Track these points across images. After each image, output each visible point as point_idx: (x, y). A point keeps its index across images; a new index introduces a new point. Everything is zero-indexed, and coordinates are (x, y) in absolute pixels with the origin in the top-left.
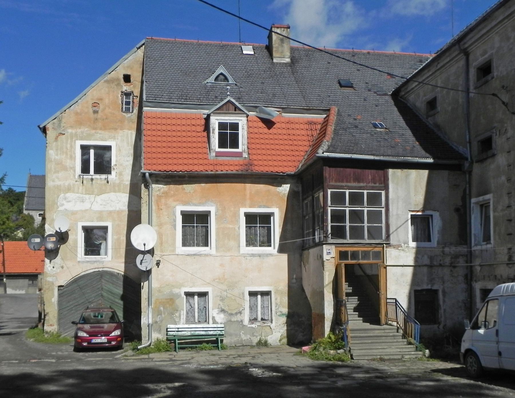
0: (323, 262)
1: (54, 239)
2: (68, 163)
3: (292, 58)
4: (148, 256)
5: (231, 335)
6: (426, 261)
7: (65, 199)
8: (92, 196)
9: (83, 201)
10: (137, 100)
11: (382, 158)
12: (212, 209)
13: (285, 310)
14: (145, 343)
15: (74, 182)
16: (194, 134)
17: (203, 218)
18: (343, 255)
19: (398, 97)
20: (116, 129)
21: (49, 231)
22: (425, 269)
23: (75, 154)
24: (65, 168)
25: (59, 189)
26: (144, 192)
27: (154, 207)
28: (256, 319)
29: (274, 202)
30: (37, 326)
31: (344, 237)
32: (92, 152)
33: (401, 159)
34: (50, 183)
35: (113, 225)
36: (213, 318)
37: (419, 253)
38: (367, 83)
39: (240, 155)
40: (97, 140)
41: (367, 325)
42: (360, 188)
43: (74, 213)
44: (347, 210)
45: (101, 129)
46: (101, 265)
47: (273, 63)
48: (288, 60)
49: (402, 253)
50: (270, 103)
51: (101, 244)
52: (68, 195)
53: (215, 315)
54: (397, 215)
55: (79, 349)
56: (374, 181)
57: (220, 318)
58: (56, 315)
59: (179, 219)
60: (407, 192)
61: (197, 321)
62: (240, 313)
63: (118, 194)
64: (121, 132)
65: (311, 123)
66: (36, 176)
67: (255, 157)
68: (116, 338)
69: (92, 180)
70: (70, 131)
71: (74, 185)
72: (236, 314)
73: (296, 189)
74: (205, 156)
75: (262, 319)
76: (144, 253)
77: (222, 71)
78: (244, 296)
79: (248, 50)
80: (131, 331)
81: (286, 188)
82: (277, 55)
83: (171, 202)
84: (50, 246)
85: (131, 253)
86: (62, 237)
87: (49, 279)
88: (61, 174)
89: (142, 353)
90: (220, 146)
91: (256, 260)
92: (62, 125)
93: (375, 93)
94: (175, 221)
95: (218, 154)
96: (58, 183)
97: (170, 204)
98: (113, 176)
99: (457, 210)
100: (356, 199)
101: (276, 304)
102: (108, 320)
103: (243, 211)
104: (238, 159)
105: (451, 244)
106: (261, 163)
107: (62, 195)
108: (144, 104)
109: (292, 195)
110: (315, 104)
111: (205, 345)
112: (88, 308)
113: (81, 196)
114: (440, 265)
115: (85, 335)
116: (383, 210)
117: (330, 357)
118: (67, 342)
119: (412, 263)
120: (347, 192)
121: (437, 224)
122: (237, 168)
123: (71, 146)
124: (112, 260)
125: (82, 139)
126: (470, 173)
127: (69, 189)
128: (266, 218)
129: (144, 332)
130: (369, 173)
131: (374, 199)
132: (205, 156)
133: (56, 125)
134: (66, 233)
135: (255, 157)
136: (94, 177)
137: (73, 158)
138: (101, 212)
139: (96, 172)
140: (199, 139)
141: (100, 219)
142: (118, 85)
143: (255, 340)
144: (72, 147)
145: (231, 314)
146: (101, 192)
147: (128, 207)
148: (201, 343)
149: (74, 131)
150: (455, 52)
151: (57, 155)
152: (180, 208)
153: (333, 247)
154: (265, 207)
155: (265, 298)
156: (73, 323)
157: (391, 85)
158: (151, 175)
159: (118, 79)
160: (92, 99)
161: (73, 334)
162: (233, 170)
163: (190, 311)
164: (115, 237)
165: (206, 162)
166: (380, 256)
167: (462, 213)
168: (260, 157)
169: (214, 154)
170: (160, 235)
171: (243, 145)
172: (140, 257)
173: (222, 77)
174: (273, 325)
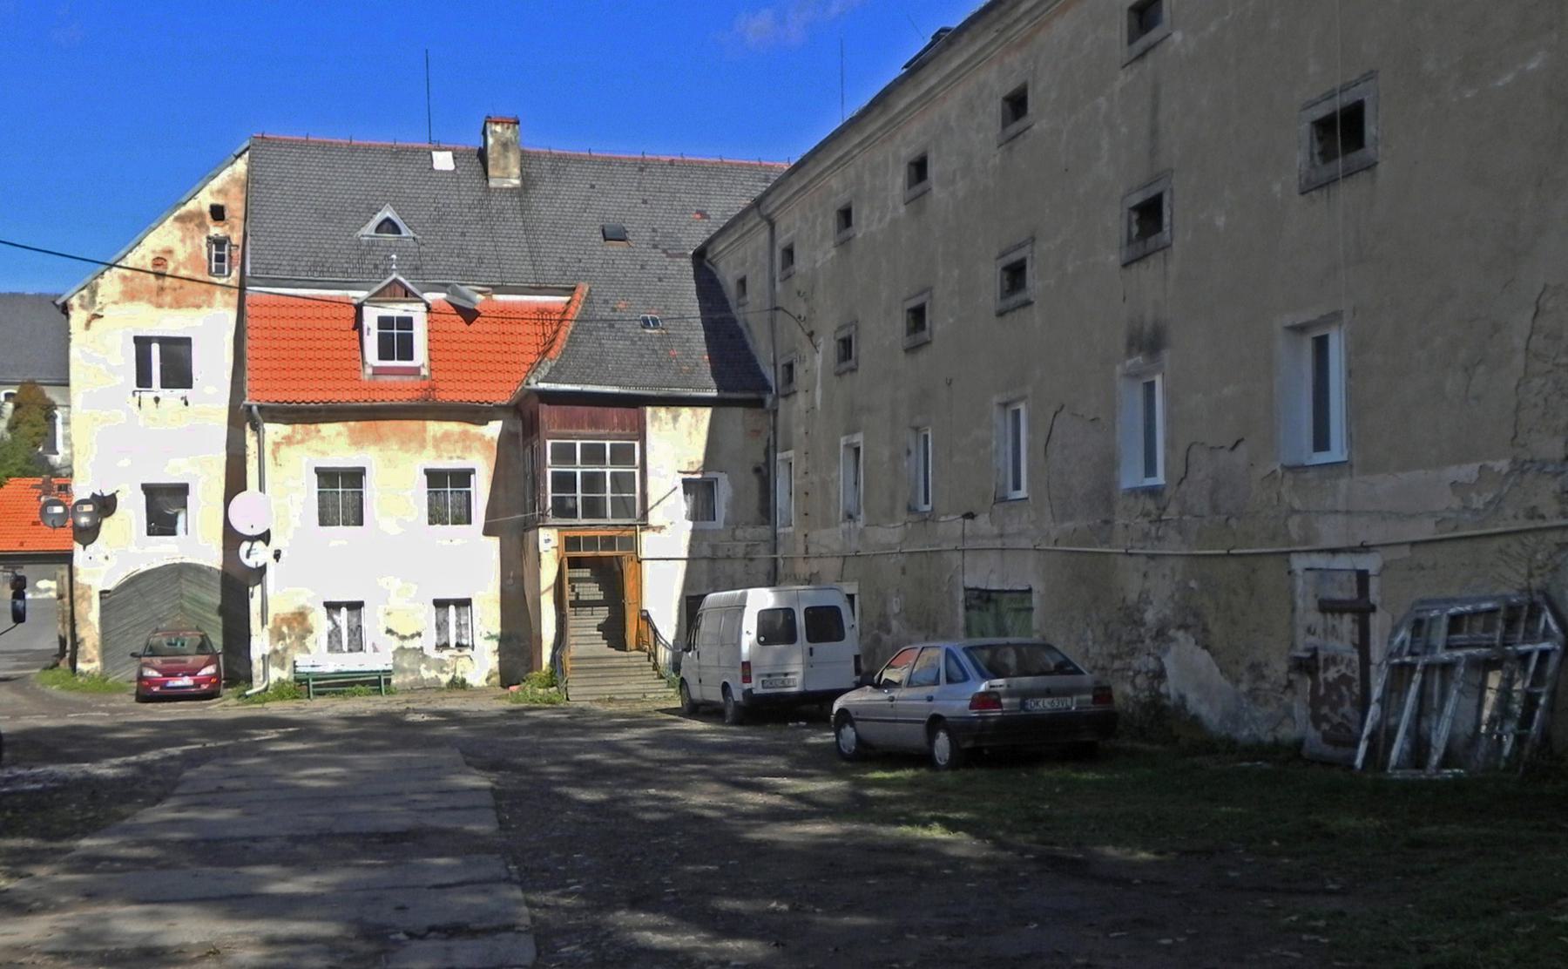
0: (539, 554)
1: (89, 508)
3: (524, 177)
4: (259, 545)
5: (404, 671)
6: (706, 551)
10: (237, 254)
11: (632, 391)
13: (497, 630)
14: (258, 686)
16: (337, 334)
17: (355, 477)
18: (571, 543)
20: (198, 307)
22: (704, 564)
26: (251, 440)
28: (446, 646)
29: (475, 450)
30: (57, 665)
32: (155, 349)
33: (664, 392)
37: (696, 536)
38: (654, 230)
39: (415, 371)
41: (613, 652)
44: (579, 472)
45: (171, 307)
47: (487, 189)
48: (516, 182)
50: (469, 275)
51: (176, 515)
55: (144, 697)
56: (622, 426)
60: (676, 443)
61: (345, 648)
65: (542, 313)
67: (441, 375)
68: (209, 678)
72: (413, 636)
73: (512, 429)
75: (459, 645)
76: (253, 539)
79: (443, 161)
80: (236, 671)
81: (494, 429)
84: (84, 520)
85: (232, 538)
86: (105, 505)
89: (253, 702)
90: (381, 358)
92: (98, 299)
93: (665, 251)
95: (378, 371)
97: (293, 461)
99: (757, 470)
100: (594, 454)
102: (195, 650)
105: (747, 524)
106: (451, 385)
108: (247, 281)
109: (505, 439)
111: (359, 687)
112: (157, 630)
114: (728, 557)
115: (155, 674)
116: (637, 472)
117: (536, 698)
118: (120, 689)
119: (685, 554)
120: (578, 443)
121: (724, 492)
122: (409, 395)
124: (198, 542)
126: (775, 412)
128: (463, 477)
129: (257, 667)
130: (614, 414)
131: (622, 455)
134: (113, 497)
135: (441, 375)
140: (345, 344)
142: (202, 225)
143: (445, 679)
145: (404, 638)
147: (228, 447)
148: (352, 684)
150: (754, 219)
153: (555, 531)
155: (462, 610)
156: (133, 655)
157: (696, 236)
158: (260, 408)
159: (200, 214)
161: (133, 674)
162: (401, 398)
163: (334, 635)
166: (631, 544)
167: (764, 475)
169: (369, 371)
172: (245, 546)
173: (389, 226)
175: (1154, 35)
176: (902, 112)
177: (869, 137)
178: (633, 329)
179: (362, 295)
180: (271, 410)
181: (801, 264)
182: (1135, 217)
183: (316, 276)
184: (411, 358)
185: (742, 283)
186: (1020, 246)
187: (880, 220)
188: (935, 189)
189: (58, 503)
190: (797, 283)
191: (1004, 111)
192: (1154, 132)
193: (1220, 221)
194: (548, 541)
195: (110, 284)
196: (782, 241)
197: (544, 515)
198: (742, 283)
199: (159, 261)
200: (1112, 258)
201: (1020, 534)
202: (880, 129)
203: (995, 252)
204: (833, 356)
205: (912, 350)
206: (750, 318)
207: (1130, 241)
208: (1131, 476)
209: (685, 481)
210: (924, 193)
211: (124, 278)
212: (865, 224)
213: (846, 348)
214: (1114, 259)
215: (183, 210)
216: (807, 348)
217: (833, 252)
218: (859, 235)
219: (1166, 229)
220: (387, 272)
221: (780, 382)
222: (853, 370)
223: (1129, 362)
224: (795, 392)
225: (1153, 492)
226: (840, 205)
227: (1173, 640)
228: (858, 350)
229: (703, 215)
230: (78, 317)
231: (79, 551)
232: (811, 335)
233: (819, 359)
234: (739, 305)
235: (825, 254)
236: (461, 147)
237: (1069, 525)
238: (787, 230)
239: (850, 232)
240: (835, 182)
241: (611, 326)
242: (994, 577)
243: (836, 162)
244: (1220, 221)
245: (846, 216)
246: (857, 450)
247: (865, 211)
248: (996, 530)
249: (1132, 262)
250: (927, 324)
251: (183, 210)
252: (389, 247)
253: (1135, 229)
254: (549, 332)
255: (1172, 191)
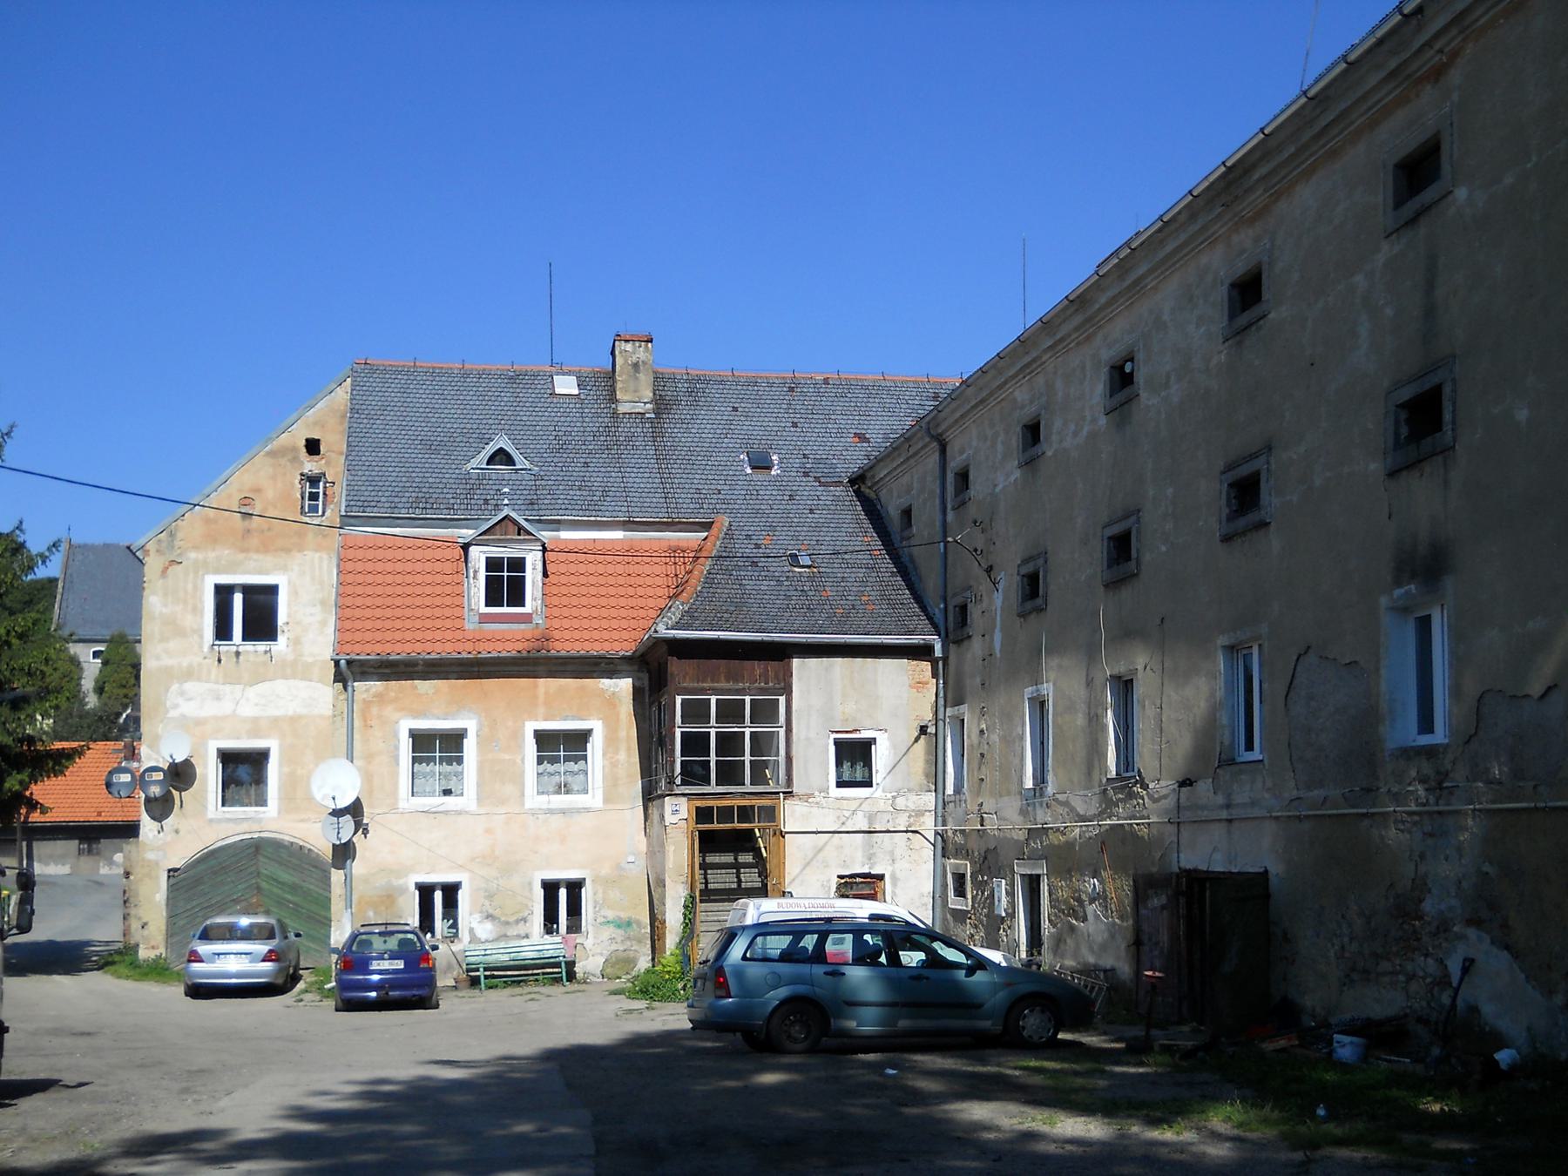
2: (188, 621)
7: (182, 693)
8: (238, 688)
9: (218, 698)
12: (467, 722)
15: (199, 659)
17: (452, 742)
18: (703, 815)
19: (862, 486)
20: (288, 551)
21: (149, 758)
23: (202, 602)
24: (181, 633)
25: (169, 675)
27: (357, 723)
31: (706, 781)
32: (238, 599)
34: (149, 665)
35: (281, 746)
36: (471, 930)
39: (527, 618)
40: (249, 573)
42: (738, 692)
43: (199, 722)
45: (257, 551)
46: (256, 827)
47: (615, 414)
49: (815, 810)
52: (188, 686)
53: (474, 925)
54: (808, 739)
57: (485, 930)
58: (164, 928)
59: (406, 744)
62: (525, 920)
63: (291, 682)
64: (299, 555)
65: (675, 551)
66: (84, 548)
67: (556, 623)
69: (238, 654)
70: (193, 555)
71: (200, 665)
72: (517, 922)
74: (458, 624)
77: (501, 445)
78: (531, 890)
79: (566, 385)
82: (626, 398)
83: (389, 711)
84: (155, 791)
86: (181, 775)
87: (151, 856)
88: (172, 645)
91: (556, 820)
92: (177, 543)
94: (397, 748)
95: (485, 618)
96: (168, 661)
98: (281, 645)
100: (731, 712)
101: (596, 902)
103: (530, 727)
104: (523, 626)
107: (175, 687)
110: (687, 511)
113: (215, 687)
116: (782, 732)
120: (713, 699)
122: (519, 646)
123: (195, 588)
125: (217, 572)
127: (189, 674)
130: (758, 667)
131: (765, 712)
132: (458, 624)
133: (164, 545)
135: (556, 623)
136: (241, 649)
137: (197, 610)
138: (255, 720)
139: (247, 636)
141: (255, 733)
142: (295, 460)
144: (198, 589)
145: (507, 923)
146: (257, 679)
149: (200, 556)
151: (165, 605)
152: (406, 725)
153: (684, 799)
154: (574, 718)
157: (854, 459)
158: (349, 662)
159: (294, 449)
160: (240, 491)
162: (508, 650)
164: (286, 770)
165: (459, 635)
166: (770, 814)
168: (566, 623)
170: (368, 778)
171: (534, 599)
174: (589, 943)
175: (1428, 195)
176: (1100, 310)
177: (1062, 340)
178: (780, 567)
179: (468, 533)
180: (362, 663)
181: (977, 489)
182: (1403, 415)
183: (418, 513)
184: (523, 605)
185: (907, 513)
186: (1253, 456)
187: (1075, 434)
188: (1143, 395)
189: (126, 770)
190: (972, 511)
191: (1230, 299)
192: (1430, 312)
193: (1522, 415)
194: (675, 812)
195: (191, 525)
196: (954, 464)
197: (671, 782)
198: (907, 513)
199: (246, 500)
200: (1372, 466)
201: (1253, 804)
202: (1076, 329)
203: (1220, 464)
204: (1015, 597)
205: (1113, 585)
206: (915, 551)
207: (1397, 445)
208: (1403, 731)
209: (837, 743)
210: (1129, 401)
211: (207, 521)
212: (1061, 438)
213: (1032, 587)
214: (1375, 467)
215: (276, 444)
216: (984, 585)
217: (1017, 474)
218: (1049, 453)
219: (1447, 427)
220: (497, 507)
221: (951, 625)
222: (1040, 610)
223: (1398, 592)
224: (969, 637)
225: (1430, 752)
226: (1025, 420)
227: (1462, 937)
228: (1046, 585)
229: (862, 438)
230: (153, 564)
231: (148, 826)
232: (989, 570)
233: (998, 599)
234: (903, 539)
235: (1008, 476)
236: (586, 370)
237: (1317, 793)
238: (962, 452)
239: (1038, 449)
240: (1021, 394)
241: (754, 564)
242: (1218, 856)
243: (1021, 370)
244: (1522, 415)
245: (1033, 432)
246: (1042, 704)
247: (1058, 424)
248: (1220, 799)
249: (1400, 470)
250: (1134, 554)
251: (276, 444)
252: (501, 481)
253: (1404, 431)
254: (681, 571)
255: (1454, 380)
